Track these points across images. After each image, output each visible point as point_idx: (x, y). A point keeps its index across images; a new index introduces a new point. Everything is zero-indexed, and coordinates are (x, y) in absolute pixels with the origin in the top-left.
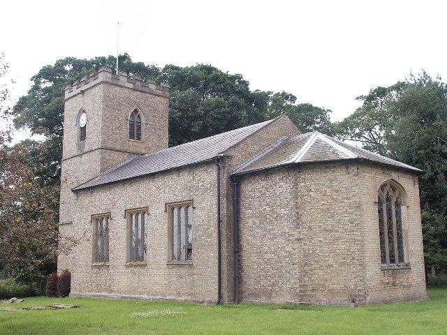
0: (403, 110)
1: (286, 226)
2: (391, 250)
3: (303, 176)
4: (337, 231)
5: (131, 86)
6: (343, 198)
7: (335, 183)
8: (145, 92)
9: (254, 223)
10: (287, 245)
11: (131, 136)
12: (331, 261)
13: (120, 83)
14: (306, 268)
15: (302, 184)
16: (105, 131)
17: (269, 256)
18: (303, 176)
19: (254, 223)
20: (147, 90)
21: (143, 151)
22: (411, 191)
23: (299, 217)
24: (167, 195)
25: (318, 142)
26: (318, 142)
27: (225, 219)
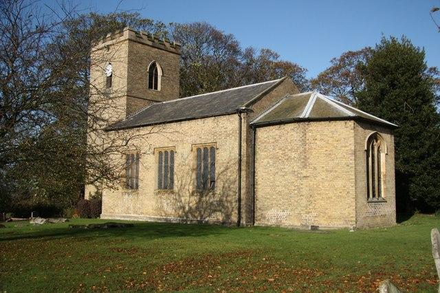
0: (429, 100)
1: (296, 166)
2: (372, 191)
3: (311, 128)
4: (336, 171)
5: (150, 43)
6: (342, 147)
7: (336, 135)
8: (161, 49)
9: (268, 163)
10: (296, 181)
11: (150, 87)
12: (331, 194)
13: (143, 41)
14: (311, 199)
15: (310, 134)
16: (131, 80)
17: (279, 189)
18: (311, 128)
19: (268, 163)
20: (163, 47)
21: (159, 99)
22: (387, 143)
23: (306, 159)
24: (193, 138)
25: (318, 99)
26: (318, 99)
27: (244, 159)
